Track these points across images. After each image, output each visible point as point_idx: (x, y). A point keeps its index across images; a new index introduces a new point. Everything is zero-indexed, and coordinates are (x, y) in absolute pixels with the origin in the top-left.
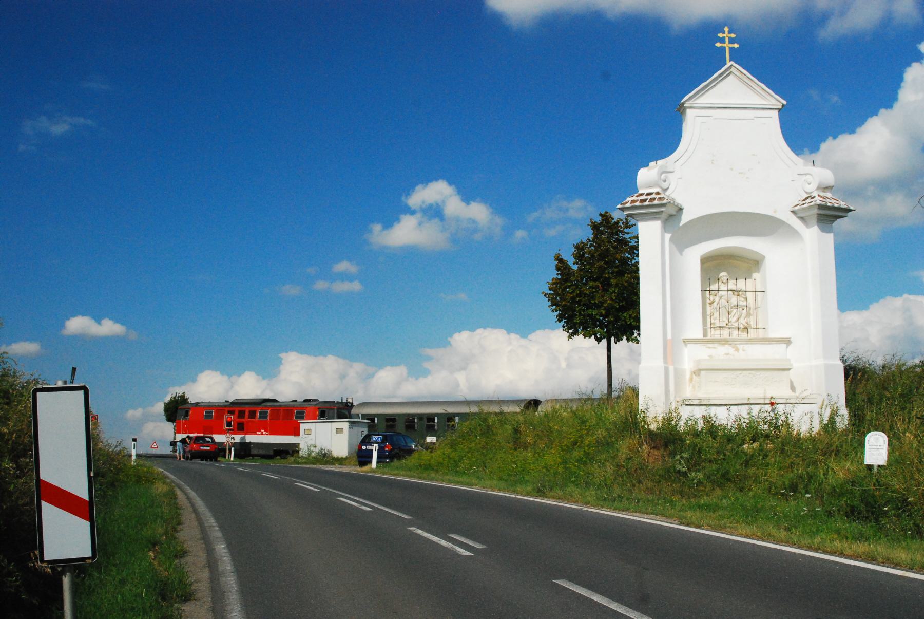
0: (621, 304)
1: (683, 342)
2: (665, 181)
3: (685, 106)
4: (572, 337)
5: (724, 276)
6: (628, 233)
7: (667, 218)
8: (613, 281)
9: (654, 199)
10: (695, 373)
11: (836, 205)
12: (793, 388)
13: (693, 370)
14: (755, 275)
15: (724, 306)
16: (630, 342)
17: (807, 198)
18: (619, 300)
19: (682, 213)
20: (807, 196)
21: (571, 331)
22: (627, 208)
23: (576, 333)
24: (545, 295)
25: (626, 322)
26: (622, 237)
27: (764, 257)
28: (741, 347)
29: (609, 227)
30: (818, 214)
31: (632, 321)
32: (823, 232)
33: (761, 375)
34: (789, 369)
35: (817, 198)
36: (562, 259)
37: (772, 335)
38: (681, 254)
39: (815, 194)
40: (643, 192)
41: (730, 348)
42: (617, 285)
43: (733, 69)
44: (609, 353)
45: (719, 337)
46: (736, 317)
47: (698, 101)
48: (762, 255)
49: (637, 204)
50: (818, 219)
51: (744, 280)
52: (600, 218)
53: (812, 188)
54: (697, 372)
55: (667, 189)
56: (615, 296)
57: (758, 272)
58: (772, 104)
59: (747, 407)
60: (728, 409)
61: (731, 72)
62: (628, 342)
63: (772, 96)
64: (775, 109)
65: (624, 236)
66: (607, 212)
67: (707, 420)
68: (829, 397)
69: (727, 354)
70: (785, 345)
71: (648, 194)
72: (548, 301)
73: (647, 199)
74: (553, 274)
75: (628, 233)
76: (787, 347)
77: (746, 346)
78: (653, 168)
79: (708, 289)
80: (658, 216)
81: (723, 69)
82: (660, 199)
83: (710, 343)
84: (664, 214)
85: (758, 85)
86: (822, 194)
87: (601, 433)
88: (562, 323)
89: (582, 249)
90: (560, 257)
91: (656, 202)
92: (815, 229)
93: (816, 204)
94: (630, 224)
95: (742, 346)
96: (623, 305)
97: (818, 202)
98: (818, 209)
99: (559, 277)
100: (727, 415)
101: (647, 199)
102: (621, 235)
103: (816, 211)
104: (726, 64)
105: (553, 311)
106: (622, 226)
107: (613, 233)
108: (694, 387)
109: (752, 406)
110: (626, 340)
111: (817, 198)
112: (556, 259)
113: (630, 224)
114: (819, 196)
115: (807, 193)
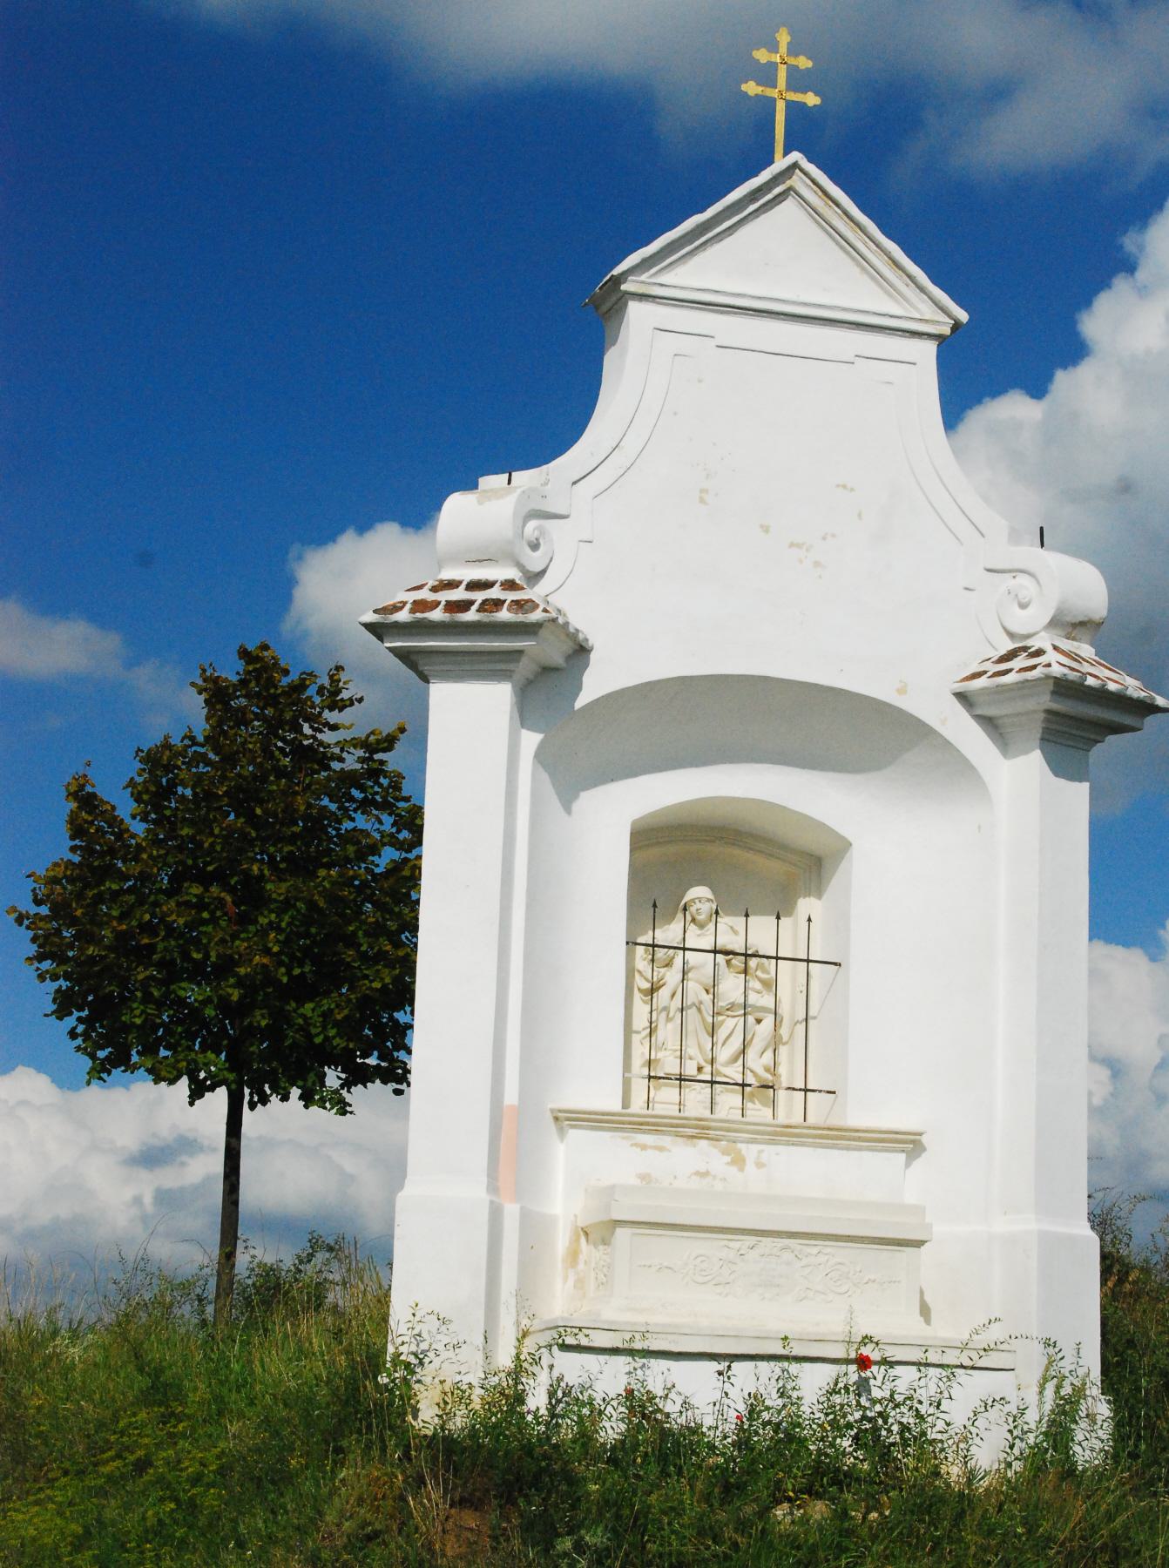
0: (297, 971)
1: (552, 1120)
2: (535, 546)
3: (623, 287)
4: (104, 1076)
5: (700, 900)
6: (334, 728)
7: (531, 677)
8: (276, 889)
9: (498, 604)
10: (586, 1234)
11: (1112, 687)
12: (925, 1312)
13: (580, 1224)
14: (806, 905)
15: (694, 1004)
16: (314, 1109)
17: (1010, 656)
18: (292, 957)
19: (586, 665)
20: (1011, 646)
21: (101, 1054)
22: (396, 625)
23: (120, 1060)
24: (20, 920)
25: (310, 1037)
26: (313, 737)
27: (844, 846)
28: (750, 1151)
29: (273, 701)
30: (1048, 712)
31: (332, 1032)
32: (1056, 774)
33: (822, 1259)
34: (919, 1244)
35: (1051, 656)
36: (94, 796)
37: (857, 1118)
38: (568, 810)
39: (1041, 641)
40: (457, 578)
41: (715, 1151)
42: (287, 905)
43: (797, 181)
44: (233, 1141)
45: (674, 1111)
46: (736, 1043)
47: (667, 278)
48: (843, 839)
49: (437, 615)
50: (1046, 731)
51: (773, 919)
52: (240, 665)
53: (1032, 621)
54: (602, 1231)
55: (543, 573)
56: (278, 941)
57: (819, 896)
58: (918, 316)
59: (776, 1367)
60: (720, 1373)
61: (790, 189)
62: (306, 1107)
63: (922, 289)
64: (930, 336)
65: (319, 736)
66: (265, 647)
67: (639, 1405)
68: (1051, 1350)
69: (704, 1175)
70: (903, 1156)
71: (475, 586)
72: (34, 940)
73: (472, 603)
74: (58, 848)
75: (334, 728)
76: (908, 1164)
77: (769, 1151)
78: (495, 494)
79: (647, 938)
80: (503, 666)
81: (765, 176)
82: (519, 605)
83: (644, 1132)
84: (524, 660)
85: (878, 245)
86: (1066, 645)
87: (237, 1433)
88: (70, 1021)
89: (168, 768)
90: (89, 789)
91: (504, 615)
92: (1033, 762)
93: (1048, 677)
94: (345, 695)
95: (755, 1148)
96: (303, 973)
97: (1057, 670)
98: (1054, 693)
99: (76, 859)
100: (717, 1395)
101: (472, 603)
102: (307, 730)
103: (1045, 701)
104: (771, 162)
105: (42, 978)
106: (317, 700)
107: (281, 723)
108: (580, 1283)
109: (794, 1368)
110: (300, 1098)
111: (1051, 656)
112: (70, 794)
113: (345, 695)
114: (1056, 648)
115: (1012, 635)
